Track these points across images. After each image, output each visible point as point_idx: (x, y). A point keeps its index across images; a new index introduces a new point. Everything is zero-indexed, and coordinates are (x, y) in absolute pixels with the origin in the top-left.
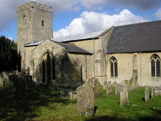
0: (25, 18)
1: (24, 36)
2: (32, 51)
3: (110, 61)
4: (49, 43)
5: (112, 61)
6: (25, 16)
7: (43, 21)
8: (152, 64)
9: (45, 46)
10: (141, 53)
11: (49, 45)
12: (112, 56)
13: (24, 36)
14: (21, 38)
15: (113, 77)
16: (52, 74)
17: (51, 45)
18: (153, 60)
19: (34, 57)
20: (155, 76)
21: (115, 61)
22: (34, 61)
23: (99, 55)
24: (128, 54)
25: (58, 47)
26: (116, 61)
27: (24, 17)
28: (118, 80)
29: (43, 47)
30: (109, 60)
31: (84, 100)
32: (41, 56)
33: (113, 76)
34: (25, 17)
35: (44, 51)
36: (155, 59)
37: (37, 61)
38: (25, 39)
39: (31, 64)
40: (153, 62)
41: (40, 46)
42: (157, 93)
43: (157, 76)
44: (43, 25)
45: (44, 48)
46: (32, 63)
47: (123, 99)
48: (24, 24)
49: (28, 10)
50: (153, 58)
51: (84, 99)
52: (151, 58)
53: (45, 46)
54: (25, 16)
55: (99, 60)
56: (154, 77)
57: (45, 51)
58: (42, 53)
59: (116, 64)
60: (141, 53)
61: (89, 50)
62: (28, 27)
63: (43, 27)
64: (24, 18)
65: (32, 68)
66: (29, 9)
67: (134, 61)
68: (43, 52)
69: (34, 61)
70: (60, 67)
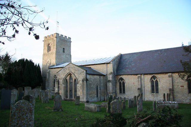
5: (121, 81)
7: (64, 49)
9: (69, 69)
18: (153, 80)
20: (154, 92)
29: (67, 69)
37: (62, 81)
44: (64, 52)
50: (153, 79)
52: (151, 79)
53: (69, 69)
56: (154, 94)
59: (124, 83)
67: (100, 77)
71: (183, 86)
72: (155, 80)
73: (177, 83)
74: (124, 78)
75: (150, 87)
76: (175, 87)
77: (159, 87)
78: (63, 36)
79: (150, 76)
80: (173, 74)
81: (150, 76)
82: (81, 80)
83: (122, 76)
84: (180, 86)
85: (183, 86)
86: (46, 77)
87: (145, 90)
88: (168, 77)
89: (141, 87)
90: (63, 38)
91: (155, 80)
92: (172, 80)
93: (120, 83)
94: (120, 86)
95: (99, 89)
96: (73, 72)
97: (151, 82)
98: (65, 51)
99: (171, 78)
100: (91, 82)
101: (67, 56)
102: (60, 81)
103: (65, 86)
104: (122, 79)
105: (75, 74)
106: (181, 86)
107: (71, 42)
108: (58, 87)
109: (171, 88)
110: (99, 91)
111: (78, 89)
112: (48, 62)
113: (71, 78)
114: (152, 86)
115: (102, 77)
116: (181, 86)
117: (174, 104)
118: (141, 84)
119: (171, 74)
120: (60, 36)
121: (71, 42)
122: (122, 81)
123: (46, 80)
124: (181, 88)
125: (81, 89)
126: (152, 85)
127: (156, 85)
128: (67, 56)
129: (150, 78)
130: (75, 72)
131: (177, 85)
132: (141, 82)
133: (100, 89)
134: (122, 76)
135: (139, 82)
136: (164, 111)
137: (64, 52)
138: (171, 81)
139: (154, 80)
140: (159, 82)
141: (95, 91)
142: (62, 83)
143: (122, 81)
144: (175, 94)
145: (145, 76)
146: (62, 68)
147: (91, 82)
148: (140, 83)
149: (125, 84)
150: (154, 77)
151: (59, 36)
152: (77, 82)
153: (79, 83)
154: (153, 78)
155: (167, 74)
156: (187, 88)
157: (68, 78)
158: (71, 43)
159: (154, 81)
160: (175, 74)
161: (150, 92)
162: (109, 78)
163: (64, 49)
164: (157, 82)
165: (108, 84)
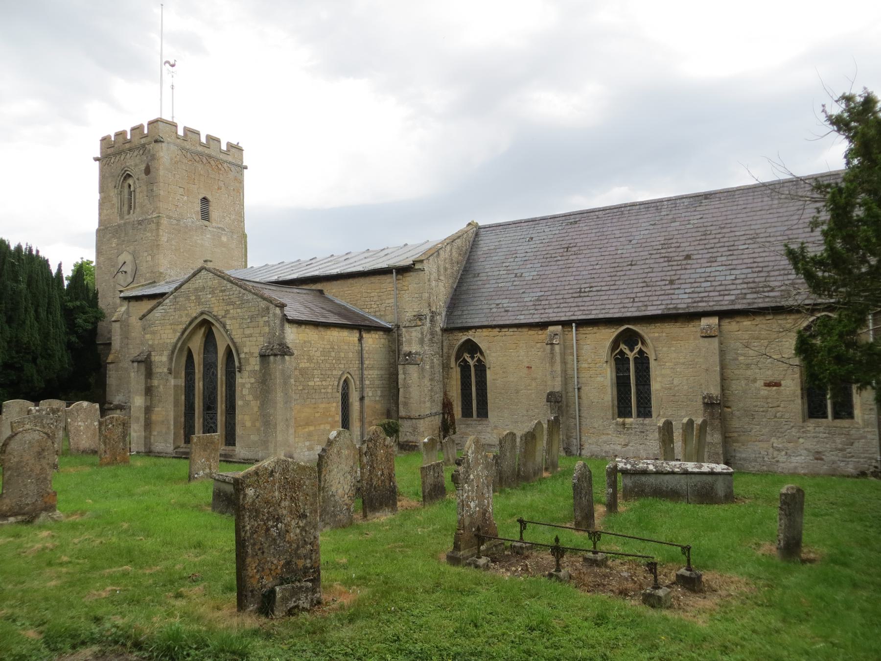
0: (130, 186)
1: (126, 257)
2: (144, 316)
3: (457, 359)
4: (210, 283)
5: (467, 356)
6: (129, 176)
7: (205, 200)
8: (618, 370)
9: (198, 298)
10: (574, 325)
11: (212, 293)
12: (464, 338)
13: (126, 257)
14: (113, 266)
15: (469, 421)
16: (221, 407)
17: (222, 291)
18: (622, 353)
19: (150, 343)
20: (629, 415)
21: (476, 359)
22: (149, 355)
23: (414, 334)
24: (525, 330)
25: (248, 301)
26: (481, 358)
27: (125, 179)
28: (489, 429)
29: (188, 298)
30: (454, 353)
31: (268, 530)
32: (179, 339)
33: (472, 416)
34: (130, 181)
35: (194, 315)
36: (632, 350)
37: (164, 359)
38: (128, 268)
39: (138, 368)
40: (621, 362)
41: (175, 298)
42: (631, 485)
43: (478, 416)
44: (205, 215)
45: (193, 305)
46: (143, 367)
47: (471, 515)
48: (126, 208)
49: (141, 152)
50: (623, 347)
51: (270, 523)
52: (615, 344)
53: (198, 298)
54: (129, 176)
55: (416, 353)
56: (628, 420)
57: (196, 318)
58: (184, 326)
59: (481, 369)
60: (574, 325)
61: (378, 314)
62: (140, 223)
63: (206, 223)
64: (126, 185)
65: (142, 387)
66: (143, 146)
67: (360, 339)
68: (186, 320)
69: (153, 358)
70: (253, 380)
71: (778, 384)
72: (636, 350)
73: (748, 366)
74: (483, 346)
75: (609, 390)
76: (736, 387)
77: (656, 386)
78: (218, 141)
79: (609, 334)
80: (726, 323)
81: (609, 334)
82: (256, 351)
83: (470, 335)
84: (760, 384)
85: (778, 384)
86: (110, 344)
87: (585, 402)
88: (699, 334)
89: (566, 380)
90: (200, 149)
91: (636, 350)
92: (722, 353)
93: (465, 369)
94: (462, 384)
95: (354, 397)
96: (218, 310)
97: (616, 360)
98: (214, 214)
99: (716, 341)
100: (310, 360)
101: (224, 239)
102: (156, 358)
103: (182, 382)
104: (471, 347)
105: (228, 322)
106: (768, 385)
107: (246, 168)
108: (149, 391)
109: (715, 391)
110: (355, 405)
111: (243, 396)
112: (124, 269)
113: (210, 340)
114: (622, 384)
115: (373, 341)
116: (768, 385)
117: (710, 479)
118: (564, 371)
119: (714, 321)
120: (181, 132)
121: (246, 168)
122: (472, 358)
123: (111, 358)
124: (765, 392)
125: (256, 398)
126: (618, 377)
127: (637, 379)
128: (224, 239)
129: (608, 344)
130: (227, 311)
131: (747, 379)
132: (564, 362)
133: (362, 399)
134: (471, 332)
135: (552, 362)
136: (245, 606)
137: (205, 215)
138: (717, 359)
139: (627, 351)
140: (652, 364)
141: (335, 408)
142: (166, 370)
143: (632, 350)
144: (735, 424)
145: (583, 330)
146: (153, 303)
147: (310, 360)
148: (558, 368)
149: (488, 372)
150: (630, 338)
151: (178, 137)
152: (237, 364)
153: (249, 368)
154: (625, 343)
155: (696, 323)
156: (799, 392)
157: (197, 344)
158: (242, 175)
159: (631, 355)
160: (738, 319)
161: (609, 414)
162: (410, 342)
163: (205, 200)
164: (643, 362)
165: (401, 371)
